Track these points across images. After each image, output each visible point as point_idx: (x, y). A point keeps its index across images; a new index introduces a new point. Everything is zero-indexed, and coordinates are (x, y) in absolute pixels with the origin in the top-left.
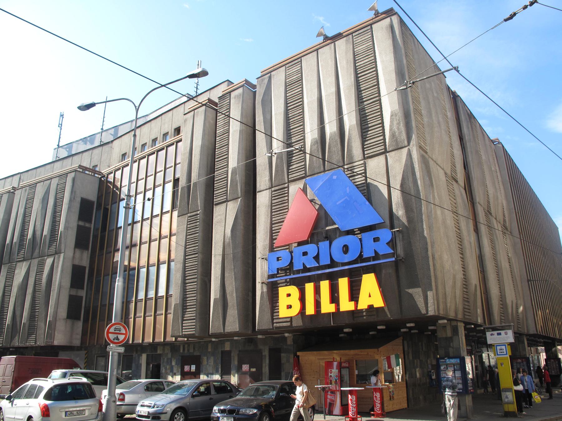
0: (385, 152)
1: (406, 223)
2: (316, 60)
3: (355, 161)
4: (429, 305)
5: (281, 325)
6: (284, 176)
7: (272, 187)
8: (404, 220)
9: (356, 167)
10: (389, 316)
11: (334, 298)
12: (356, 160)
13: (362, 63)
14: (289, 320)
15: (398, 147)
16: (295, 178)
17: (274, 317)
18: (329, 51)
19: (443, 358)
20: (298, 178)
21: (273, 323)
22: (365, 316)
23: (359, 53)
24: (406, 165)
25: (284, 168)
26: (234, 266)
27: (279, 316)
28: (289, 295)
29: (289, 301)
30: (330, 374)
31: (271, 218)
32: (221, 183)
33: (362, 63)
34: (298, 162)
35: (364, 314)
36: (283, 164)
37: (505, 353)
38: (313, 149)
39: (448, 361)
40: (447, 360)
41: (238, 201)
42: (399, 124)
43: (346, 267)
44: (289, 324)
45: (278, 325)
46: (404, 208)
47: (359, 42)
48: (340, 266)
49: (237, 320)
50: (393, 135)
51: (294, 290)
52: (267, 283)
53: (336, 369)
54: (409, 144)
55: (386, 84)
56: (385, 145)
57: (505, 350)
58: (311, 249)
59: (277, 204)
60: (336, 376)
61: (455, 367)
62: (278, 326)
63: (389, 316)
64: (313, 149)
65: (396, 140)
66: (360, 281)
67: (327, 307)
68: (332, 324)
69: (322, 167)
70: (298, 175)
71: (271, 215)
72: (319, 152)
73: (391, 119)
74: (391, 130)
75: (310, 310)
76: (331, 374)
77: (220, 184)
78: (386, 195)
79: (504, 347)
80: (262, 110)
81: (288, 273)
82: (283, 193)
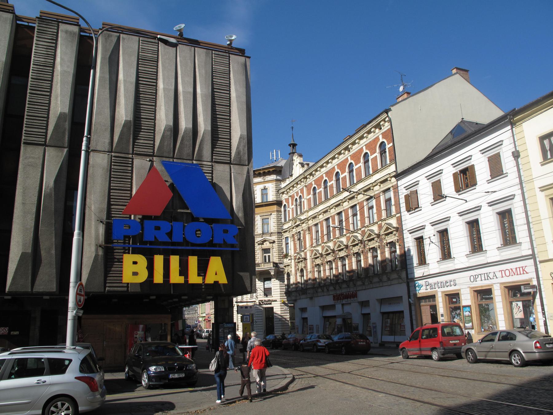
0: (153, 156)
1: (244, 224)
2: (175, 52)
3: (203, 160)
4: (253, 286)
5: (116, 289)
6: (129, 146)
7: (112, 152)
8: (242, 221)
9: (205, 166)
10: (223, 291)
11: (184, 271)
12: (205, 160)
13: (219, 81)
14: (126, 285)
15: (241, 164)
16: (141, 153)
17: (107, 281)
18: (188, 51)
19: (222, 323)
20: (145, 154)
21: (105, 287)
22: (203, 289)
23: (217, 71)
24: (246, 180)
25: (130, 139)
26: (55, 221)
27: (122, 280)
28: (135, 263)
29: (135, 268)
30: (135, 336)
31: (110, 183)
32: (37, 121)
33: (219, 81)
34: (146, 139)
35: (203, 287)
36: (130, 135)
37: (249, 321)
38: (166, 134)
39: (225, 325)
40: (225, 325)
41: (63, 151)
42: (244, 146)
43: (198, 248)
44: (125, 289)
45: (112, 289)
46: (243, 212)
47: (217, 62)
48: (190, 245)
49: (55, 280)
50: (238, 153)
51: (142, 260)
52: (103, 247)
53: (142, 331)
54: (248, 165)
55: (238, 110)
56: (46, 139)
57: (249, 319)
58: (165, 226)
59: (118, 170)
60: (142, 338)
61: (230, 330)
62: (112, 290)
63: (223, 291)
64: (166, 134)
65: (240, 158)
66: (208, 261)
67: (176, 278)
68: (172, 293)
69: (172, 153)
70: (146, 151)
71: (110, 181)
72: (171, 139)
73: (239, 140)
74: (238, 148)
75: (158, 278)
76: (136, 336)
77: (35, 121)
78: (229, 198)
79: (248, 317)
80: (108, 66)
81: (127, 240)
82: (127, 162)
